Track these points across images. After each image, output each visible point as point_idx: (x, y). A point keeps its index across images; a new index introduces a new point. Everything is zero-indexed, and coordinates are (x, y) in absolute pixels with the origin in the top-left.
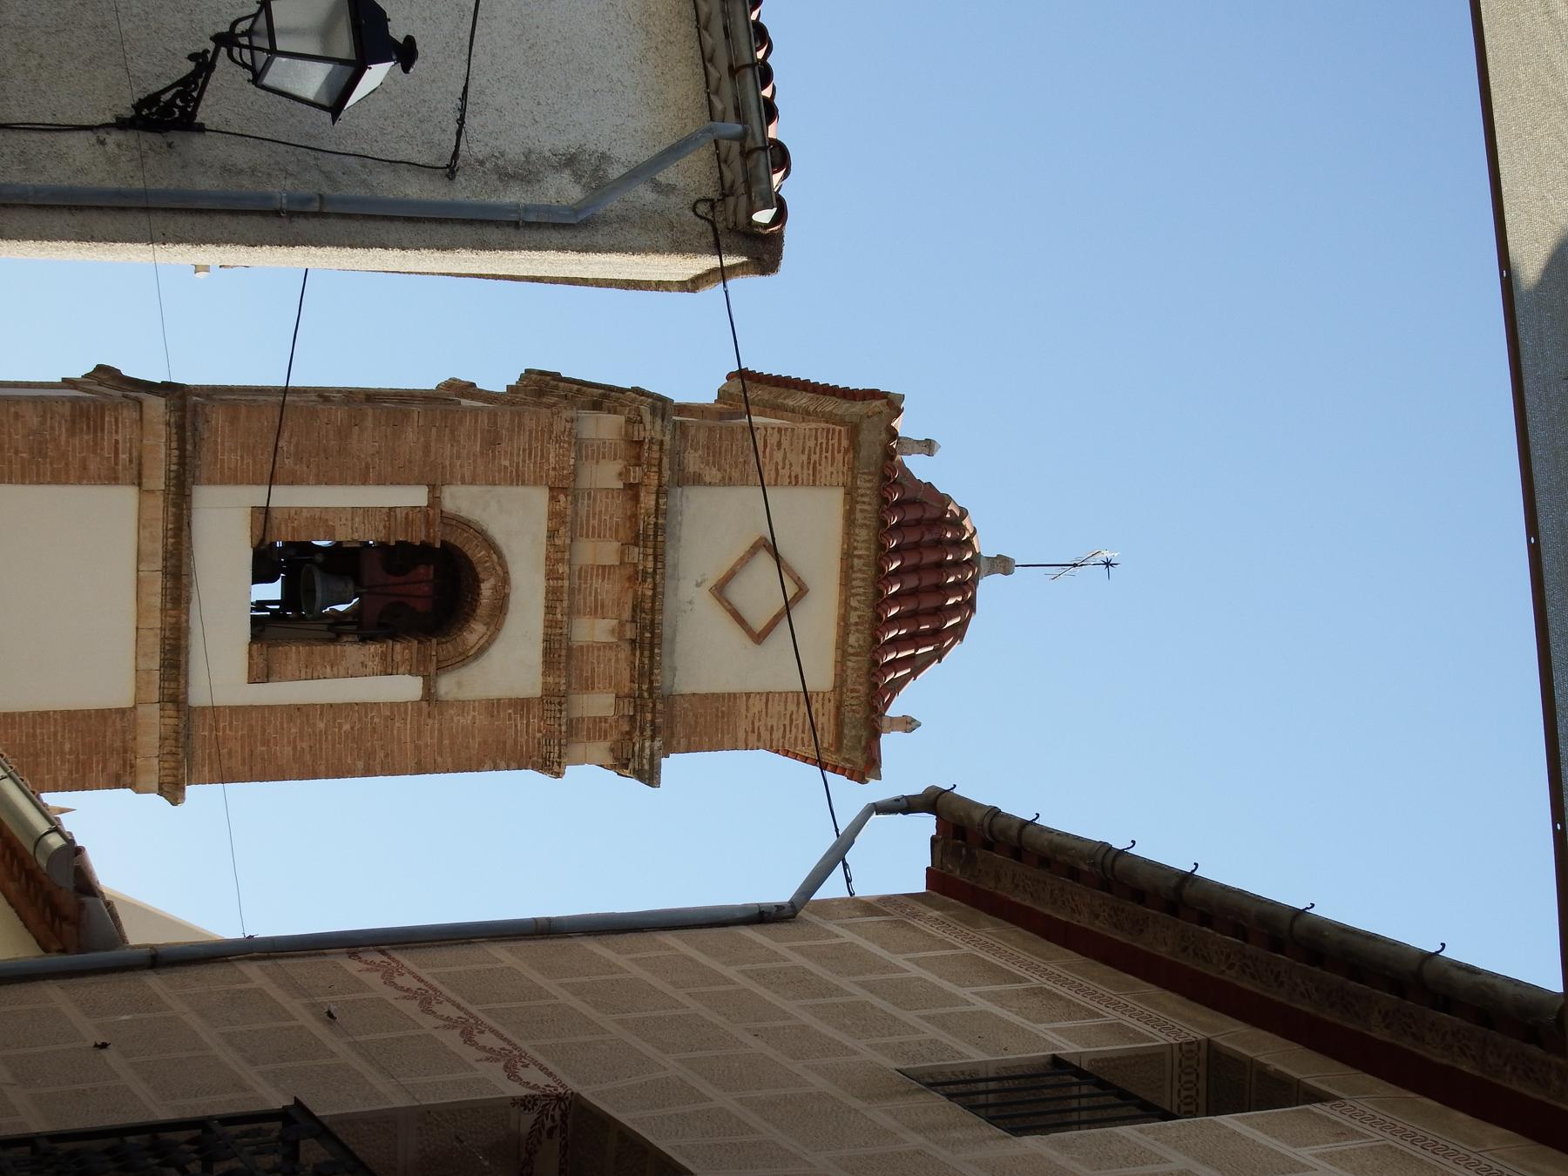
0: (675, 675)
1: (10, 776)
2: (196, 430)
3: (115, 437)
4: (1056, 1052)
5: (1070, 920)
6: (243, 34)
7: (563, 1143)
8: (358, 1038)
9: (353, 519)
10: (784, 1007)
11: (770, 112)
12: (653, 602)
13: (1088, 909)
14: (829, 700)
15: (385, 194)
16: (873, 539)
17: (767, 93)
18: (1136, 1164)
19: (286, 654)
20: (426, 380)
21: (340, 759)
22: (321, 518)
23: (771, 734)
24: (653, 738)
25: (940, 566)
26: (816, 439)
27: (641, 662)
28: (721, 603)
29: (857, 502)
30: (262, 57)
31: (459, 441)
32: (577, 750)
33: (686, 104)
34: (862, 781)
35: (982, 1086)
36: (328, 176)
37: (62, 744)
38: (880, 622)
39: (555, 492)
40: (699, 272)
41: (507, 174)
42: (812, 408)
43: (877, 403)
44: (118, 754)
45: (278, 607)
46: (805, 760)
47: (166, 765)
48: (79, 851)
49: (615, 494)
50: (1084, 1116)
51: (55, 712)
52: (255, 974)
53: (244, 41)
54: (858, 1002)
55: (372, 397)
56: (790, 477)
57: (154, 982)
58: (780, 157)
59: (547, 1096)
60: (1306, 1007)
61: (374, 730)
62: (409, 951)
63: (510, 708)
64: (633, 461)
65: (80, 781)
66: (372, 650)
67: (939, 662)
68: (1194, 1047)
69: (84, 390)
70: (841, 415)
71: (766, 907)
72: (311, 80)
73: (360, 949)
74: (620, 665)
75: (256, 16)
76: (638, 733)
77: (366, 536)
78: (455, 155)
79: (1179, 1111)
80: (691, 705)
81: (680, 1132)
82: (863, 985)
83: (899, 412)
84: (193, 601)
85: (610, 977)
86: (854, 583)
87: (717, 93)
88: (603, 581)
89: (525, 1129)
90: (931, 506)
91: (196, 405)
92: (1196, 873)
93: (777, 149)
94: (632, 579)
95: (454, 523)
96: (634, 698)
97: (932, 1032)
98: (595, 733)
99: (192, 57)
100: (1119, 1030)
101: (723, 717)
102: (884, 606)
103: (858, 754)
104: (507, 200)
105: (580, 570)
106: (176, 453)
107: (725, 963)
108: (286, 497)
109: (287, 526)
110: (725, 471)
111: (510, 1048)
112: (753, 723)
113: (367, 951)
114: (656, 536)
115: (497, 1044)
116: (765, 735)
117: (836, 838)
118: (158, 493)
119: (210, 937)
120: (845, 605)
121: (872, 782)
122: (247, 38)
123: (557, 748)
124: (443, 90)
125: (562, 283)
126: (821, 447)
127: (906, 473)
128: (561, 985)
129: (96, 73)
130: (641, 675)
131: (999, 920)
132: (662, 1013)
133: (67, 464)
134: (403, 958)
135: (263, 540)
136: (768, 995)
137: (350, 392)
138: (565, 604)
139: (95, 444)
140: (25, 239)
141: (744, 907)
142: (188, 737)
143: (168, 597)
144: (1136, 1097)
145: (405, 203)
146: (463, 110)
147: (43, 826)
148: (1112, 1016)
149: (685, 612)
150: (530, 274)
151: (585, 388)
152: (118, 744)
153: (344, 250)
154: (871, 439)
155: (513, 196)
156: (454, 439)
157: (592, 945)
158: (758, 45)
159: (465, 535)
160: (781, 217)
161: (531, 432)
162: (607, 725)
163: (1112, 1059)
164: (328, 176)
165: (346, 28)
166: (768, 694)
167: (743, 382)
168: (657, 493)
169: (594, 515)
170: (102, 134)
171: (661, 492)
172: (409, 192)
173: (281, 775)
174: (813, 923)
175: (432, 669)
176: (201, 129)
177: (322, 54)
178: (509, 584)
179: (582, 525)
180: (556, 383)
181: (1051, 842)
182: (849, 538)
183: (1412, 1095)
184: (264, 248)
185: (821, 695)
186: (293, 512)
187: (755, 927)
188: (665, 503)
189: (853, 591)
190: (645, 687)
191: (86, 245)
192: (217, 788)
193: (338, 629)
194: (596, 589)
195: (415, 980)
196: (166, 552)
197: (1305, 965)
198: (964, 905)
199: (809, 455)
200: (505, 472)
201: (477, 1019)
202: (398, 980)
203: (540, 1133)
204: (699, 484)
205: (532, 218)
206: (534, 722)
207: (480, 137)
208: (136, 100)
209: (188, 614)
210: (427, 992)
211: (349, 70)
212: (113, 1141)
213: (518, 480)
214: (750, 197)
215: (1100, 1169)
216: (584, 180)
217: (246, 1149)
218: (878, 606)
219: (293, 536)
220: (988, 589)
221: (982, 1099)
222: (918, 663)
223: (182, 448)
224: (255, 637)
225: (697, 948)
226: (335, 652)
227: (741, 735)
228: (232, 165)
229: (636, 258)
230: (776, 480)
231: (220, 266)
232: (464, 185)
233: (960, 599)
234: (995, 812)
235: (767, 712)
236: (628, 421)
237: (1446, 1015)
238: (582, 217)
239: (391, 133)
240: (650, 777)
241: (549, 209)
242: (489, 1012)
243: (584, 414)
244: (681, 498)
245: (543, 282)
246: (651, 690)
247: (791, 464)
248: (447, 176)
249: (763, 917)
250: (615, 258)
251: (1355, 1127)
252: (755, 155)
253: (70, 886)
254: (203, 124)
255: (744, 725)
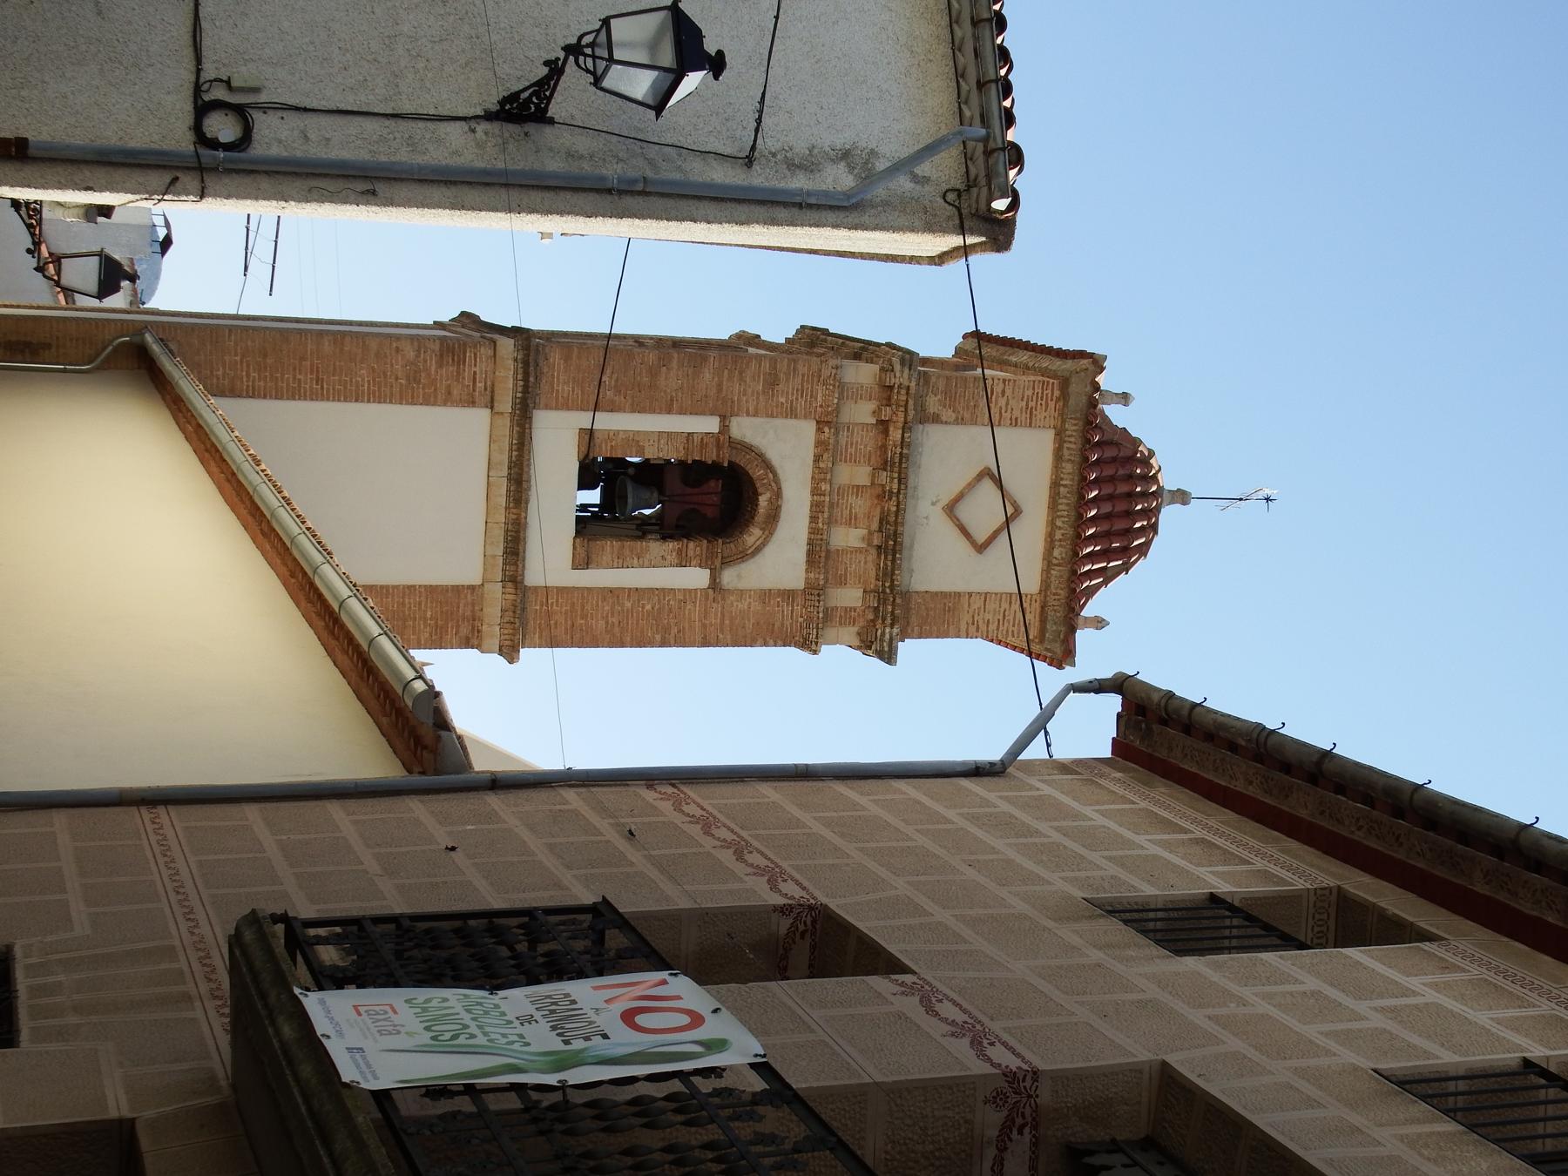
0: (912, 576)
1: (386, 634)
2: (538, 365)
3: (474, 369)
4: (1525, 1055)
5: (1229, 785)
6: (588, 46)
7: (813, 943)
8: (653, 853)
9: (659, 441)
10: (992, 844)
11: (1009, 119)
12: (897, 516)
13: (1241, 777)
14: (1036, 601)
15: (696, 178)
16: (1077, 471)
17: (1007, 103)
18: (1276, 983)
19: (603, 547)
20: (721, 331)
21: (642, 632)
22: (634, 440)
23: (988, 627)
24: (892, 626)
25: (1131, 496)
26: (1034, 389)
27: (885, 564)
28: (951, 518)
29: (1065, 442)
30: (602, 65)
31: (745, 382)
32: (831, 632)
33: (941, 111)
34: (1060, 667)
35: (1152, 915)
36: (651, 162)
37: (425, 611)
38: (1079, 540)
39: (821, 424)
40: (945, 249)
41: (793, 165)
42: (1031, 364)
43: (1085, 361)
44: (468, 621)
45: (597, 509)
46: (1014, 648)
47: (506, 632)
48: (437, 695)
49: (869, 428)
50: (1234, 942)
51: (420, 586)
52: (572, 798)
53: (588, 51)
54: (1053, 843)
55: (677, 344)
56: (1011, 419)
57: (494, 800)
58: (1016, 156)
59: (801, 905)
60: (1421, 864)
61: (670, 611)
62: (694, 786)
63: (778, 597)
64: (884, 402)
65: (437, 642)
66: (671, 546)
67: (1126, 574)
68: (1327, 892)
69: (450, 331)
70: (1055, 371)
71: (981, 764)
72: (640, 84)
73: (656, 782)
74: (867, 566)
75: (598, 31)
76: (880, 621)
77: (670, 454)
78: (753, 148)
79: (1312, 942)
80: (924, 600)
81: (907, 939)
82: (1057, 829)
83: (1102, 369)
84: (531, 500)
85: (854, 813)
86: (1060, 507)
87: (966, 103)
88: (857, 498)
89: (783, 931)
90: (1126, 447)
91: (538, 345)
92: (1334, 751)
93: (1014, 150)
94: (880, 497)
95: (739, 446)
96: (878, 593)
97: (1114, 870)
98: (846, 620)
99: (546, 63)
100: (1266, 876)
101: (949, 611)
102: (1084, 527)
103: (1058, 645)
104: (793, 186)
105: (839, 488)
106: (521, 383)
107: (946, 807)
108: (607, 422)
109: (606, 446)
110: (959, 412)
111: (773, 866)
112: (973, 617)
113: (661, 784)
114: (901, 463)
115: (763, 862)
116: (983, 627)
117: (1039, 711)
118: (506, 415)
119: (530, 767)
120: (1052, 524)
121: (1068, 668)
122: (590, 49)
123: (815, 630)
124: (745, 95)
125: (834, 255)
126: (1037, 396)
127: (1106, 419)
128: (815, 818)
129: (470, 75)
130: (885, 574)
131: (1171, 783)
132: (894, 844)
133: (435, 390)
134: (690, 791)
135: (587, 456)
136: (980, 834)
137: (660, 339)
138: (826, 515)
139: (458, 373)
140: (410, 206)
141: (964, 763)
142: (523, 609)
143: (511, 499)
144: (1277, 930)
145: (711, 186)
146: (761, 112)
147: (410, 674)
148: (1260, 864)
149: (922, 525)
150: (809, 247)
151: (847, 342)
152: (468, 613)
153: (661, 222)
154: (1078, 389)
155: (799, 182)
156: (742, 379)
157: (840, 788)
158: (1002, 64)
159: (748, 457)
160: (1014, 205)
161: (803, 376)
162: (856, 614)
163: (1259, 899)
164: (651, 162)
165: (670, 44)
166: (986, 594)
167: (979, 342)
168: (903, 428)
169: (852, 444)
170: (473, 124)
171: (906, 427)
172: (715, 177)
173: (595, 643)
174: (1018, 778)
175: (718, 563)
176: (551, 121)
177: (650, 63)
178: (782, 498)
179: (841, 452)
180: (824, 337)
181: (1215, 721)
182: (1057, 471)
183: (1506, 939)
184: (598, 219)
185: (1029, 596)
186: (611, 434)
187: (973, 779)
188: (910, 437)
189: (1059, 513)
190: (887, 584)
191: (458, 212)
192: (546, 652)
193: (643, 529)
194: (851, 504)
195: (698, 809)
196: (510, 462)
197: (1421, 830)
198: (1141, 769)
199: (1027, 402)
200: (782, 407)
201: (747, 842)
202: (685, 808)
203: (795, 934)
204: (937, 422)
205: (813, 201)
206: (798, 609)
207: (774, 134)
208: (501, 97)
209: (526, 513)
210: (679, 795)
211: (671, 77)
212: (458, 924)
213: (791, 414)
214: (990, 188)
215: (1246, 986)
216: (856, 171)
217: (565, 934)
218: (1079, 526)
219: (611, 453)
220: (1169, 516)
221: (1151, 925)
222: (1109, 573)
223: (526, 379)
224: (578, 533)
225: (924, 794)
226: (641, 547)
227: (963, 627)
228: (576, 152)
229: (896, 236)
230: (1000, 422)
231: (562, 234)
232: (759, 172)
233: (1145, 523)
234: (1170, 695)
235: (985, 608)
236: (882, 369)
237: (1536, 875)
238: (854, 201)
239: (703, 128)
240: (889, 656)
241: (826, 194)
242: (756, 837)
243: (846, 362)
244: (922, 433)
245: (818, 254)
246: (892, 587)
247: (1012, 409)
248: (746, 165)
249: (978, 771)
250: (878, 235)
251: (1457, 962)
252: (996, 155)
253: (430, 722)
254: (553, 118)
255: (966, 618)
